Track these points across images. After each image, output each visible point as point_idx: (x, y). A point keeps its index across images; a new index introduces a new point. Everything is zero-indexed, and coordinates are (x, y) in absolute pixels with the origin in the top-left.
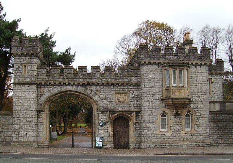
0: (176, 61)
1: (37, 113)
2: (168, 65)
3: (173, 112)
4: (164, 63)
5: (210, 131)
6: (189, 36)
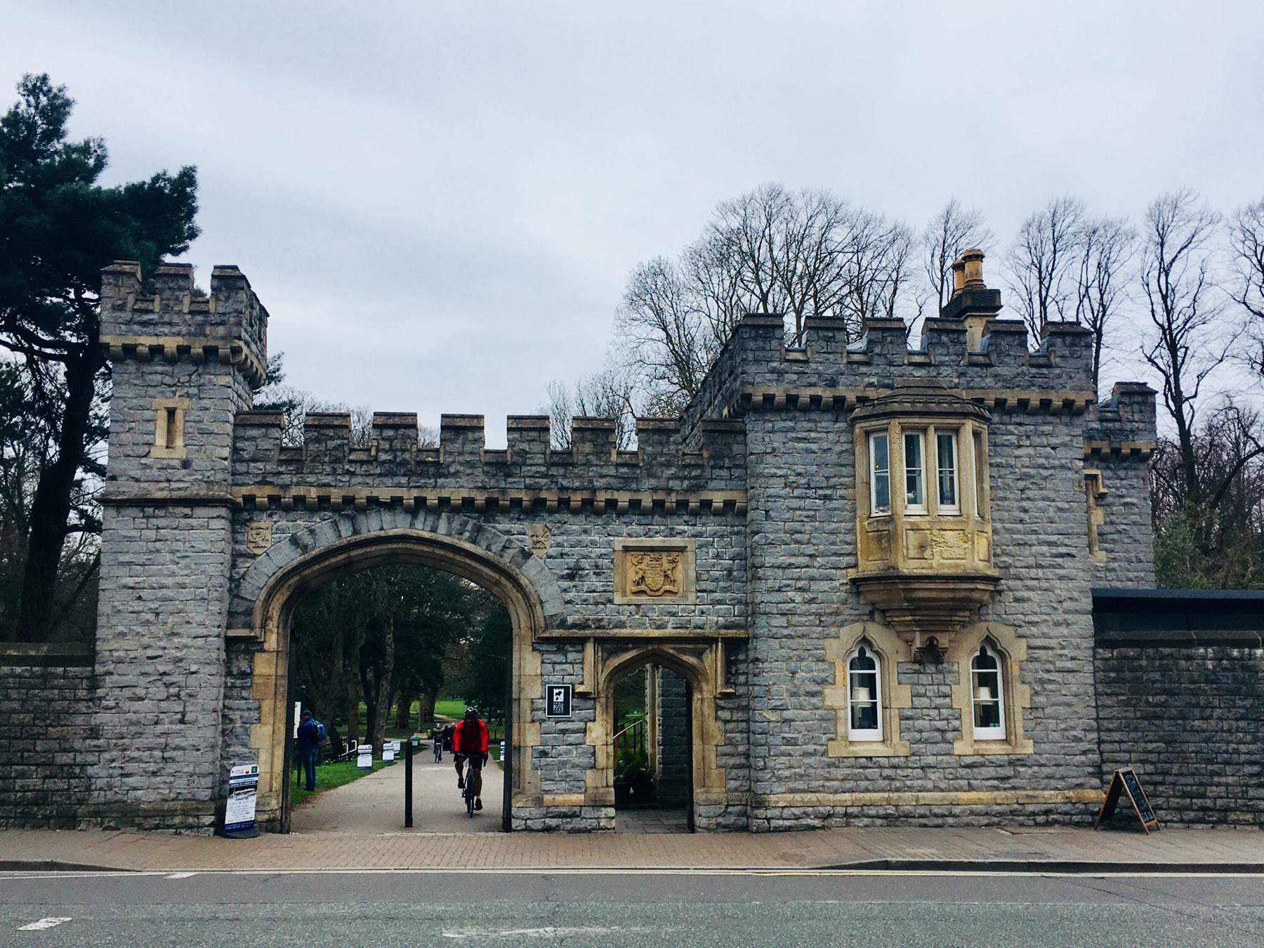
0: (922, 391)
1: (227, 650)
2: (880, 409)
3: (909, 643)
4: (862, 400)
5: (1100, 742)
6: (978, 273)
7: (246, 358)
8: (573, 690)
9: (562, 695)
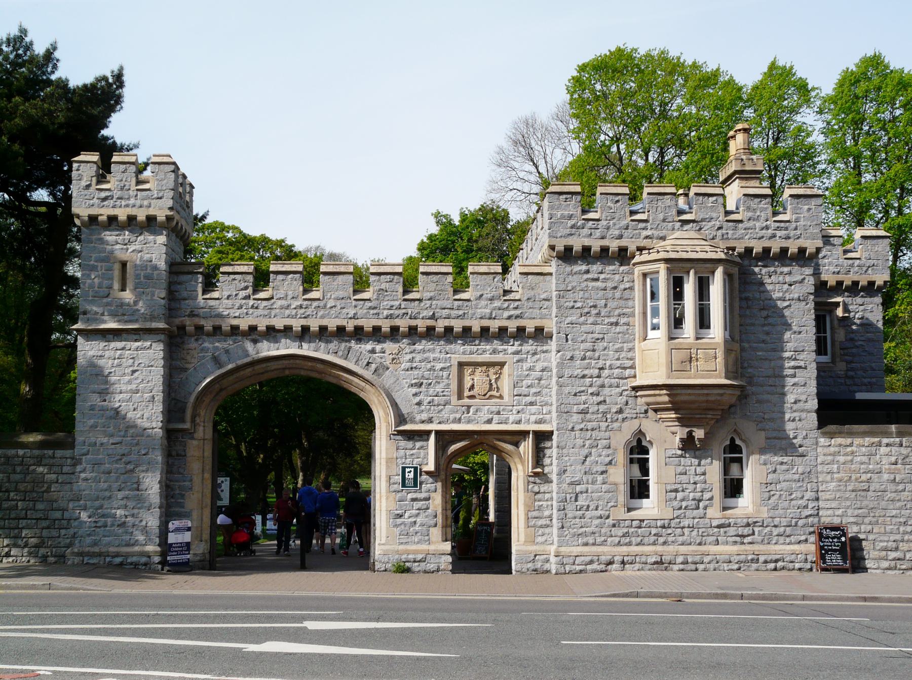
7: (177, 223)
8: (420, 469)
9: (412, 473)
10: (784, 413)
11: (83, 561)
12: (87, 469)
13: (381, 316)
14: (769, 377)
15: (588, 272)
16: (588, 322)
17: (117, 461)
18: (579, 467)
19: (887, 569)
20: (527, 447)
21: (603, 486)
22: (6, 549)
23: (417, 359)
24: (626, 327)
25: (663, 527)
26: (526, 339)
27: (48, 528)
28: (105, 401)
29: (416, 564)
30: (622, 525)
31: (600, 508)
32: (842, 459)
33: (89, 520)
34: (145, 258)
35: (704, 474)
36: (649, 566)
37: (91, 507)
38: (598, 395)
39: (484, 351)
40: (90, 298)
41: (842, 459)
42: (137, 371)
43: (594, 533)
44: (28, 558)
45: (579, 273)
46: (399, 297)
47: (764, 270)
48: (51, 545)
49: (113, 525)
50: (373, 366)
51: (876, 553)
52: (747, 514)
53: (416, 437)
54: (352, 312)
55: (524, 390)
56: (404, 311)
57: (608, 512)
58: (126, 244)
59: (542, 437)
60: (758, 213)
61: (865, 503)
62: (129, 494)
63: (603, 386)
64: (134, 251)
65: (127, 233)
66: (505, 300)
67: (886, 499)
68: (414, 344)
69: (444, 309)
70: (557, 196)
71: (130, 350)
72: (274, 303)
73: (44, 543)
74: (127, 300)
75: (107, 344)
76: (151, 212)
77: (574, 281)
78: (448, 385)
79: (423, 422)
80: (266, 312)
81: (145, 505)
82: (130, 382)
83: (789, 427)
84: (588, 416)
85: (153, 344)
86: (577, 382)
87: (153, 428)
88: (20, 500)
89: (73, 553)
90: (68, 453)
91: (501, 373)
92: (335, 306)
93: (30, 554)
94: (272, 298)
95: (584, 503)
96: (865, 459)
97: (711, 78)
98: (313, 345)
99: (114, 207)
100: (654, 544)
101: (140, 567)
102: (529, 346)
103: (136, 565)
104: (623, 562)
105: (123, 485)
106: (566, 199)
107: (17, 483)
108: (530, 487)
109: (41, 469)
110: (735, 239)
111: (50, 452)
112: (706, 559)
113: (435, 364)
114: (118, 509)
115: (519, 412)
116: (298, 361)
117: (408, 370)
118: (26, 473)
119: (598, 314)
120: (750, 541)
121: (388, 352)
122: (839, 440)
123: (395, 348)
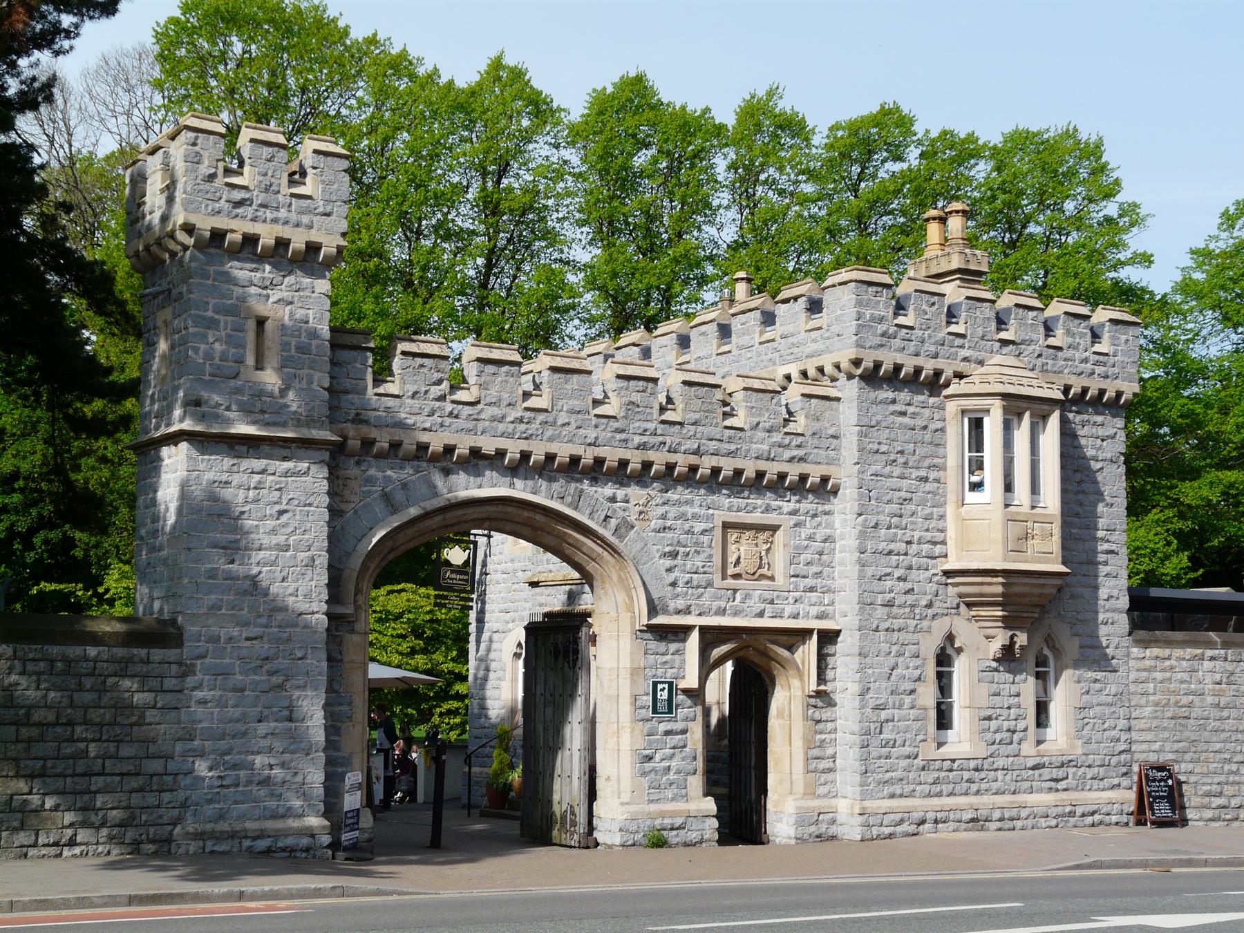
9: (666, 691)
10: (1097, 613)
11: (204, 848)
12: (205, 683)
13: (629, 445)
14: (1081, 563)
15: (894, 402)
16: (894, 474)
17: (255, 670)
18: (884, 684)
19: (1211, 820)
20: (808, 652)
21: (912, 711)
22: (69, 832)
23: (671, 515)
24: (936, 485)
25: (976, 770)
26: (805, 493)
27: (141, 790)
28: (232, 562)
29: (674, 833)
30: (932, 768)
31: (907, 744)
32: (1159, 676)
33: (210, 774)
34: (297, 316)
35: (1018, 695)
36: (964, 826)
37: (214, 751)
38: (905, 580)
39: (755, 508)
40: (207, 378)
41: (1159, 676)
42: (286, 511)
43: (901, 780)
44: (108, 847)
45: (884, 402)
46: (655, 417)
47: (1079, 418)
48: (146, 821)
49: (249, 782)
50: (613, 523)
51: (1199, 799)
52: (1060, 750)
53: (670, 636)
54: (592, 434)
55: (802, 569)
56: (661, 439)
57: (916, 749)
58: (266, 288)
59: (828, 638)
60: (1077, 340)
61: (1186, 734)
62: (276, 728)
63: (910, 568)
64: (279, 300)
65: (268, 268)
66: (786, 434)
67: (1209, 728)
68: (666, 492)
69: (711, 440)
70: (865, 287)
71: (274, 474)
72: (482, 410)
73: (134, 818)
74: (269, 388)
75: (235, 461)
76: (315, 236)
77: (879, 413)
78: (711, 556)
79: (679, 612)
80: (470, 425)
81: (303, 745)
82: (273, 531)
83: (1103, 630)
84: (895, 610)
85: (312, 467)
86: (883, 561)
87: (313, 613)
88: (93, 740)
89: (188, 833)
90: (172, 654)
91: (772, 543)
92: (568, 424)
93: (111, 838)
94: (478, 402)
95: (890, 737)
96: (1186, 676)
97: (401, 64)
98: (530, 483)
99: (254, 220)
100: (966, 794)
101: (298, 854)
102: (808, 504)
103: (291, 851)
104: (936, 821)
105: (266, 712)
106: (877, 292)
107: (86, 708)
108: (811, 712)
109: (127, 683)
110: (1055, 372)
111: (143, 652)
112: (1024, 814)
113: (695, 524)
114: (259, 753)
115: (796, 601)
116: (509, 509)
117: (659, 532)
118: (102, 690)
119: (905, 463)
120: (1065, 787)
121: (633, 502)
122: (1156, 651)
123: (642, 496)
